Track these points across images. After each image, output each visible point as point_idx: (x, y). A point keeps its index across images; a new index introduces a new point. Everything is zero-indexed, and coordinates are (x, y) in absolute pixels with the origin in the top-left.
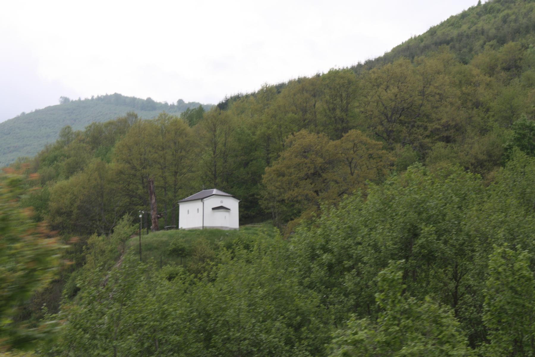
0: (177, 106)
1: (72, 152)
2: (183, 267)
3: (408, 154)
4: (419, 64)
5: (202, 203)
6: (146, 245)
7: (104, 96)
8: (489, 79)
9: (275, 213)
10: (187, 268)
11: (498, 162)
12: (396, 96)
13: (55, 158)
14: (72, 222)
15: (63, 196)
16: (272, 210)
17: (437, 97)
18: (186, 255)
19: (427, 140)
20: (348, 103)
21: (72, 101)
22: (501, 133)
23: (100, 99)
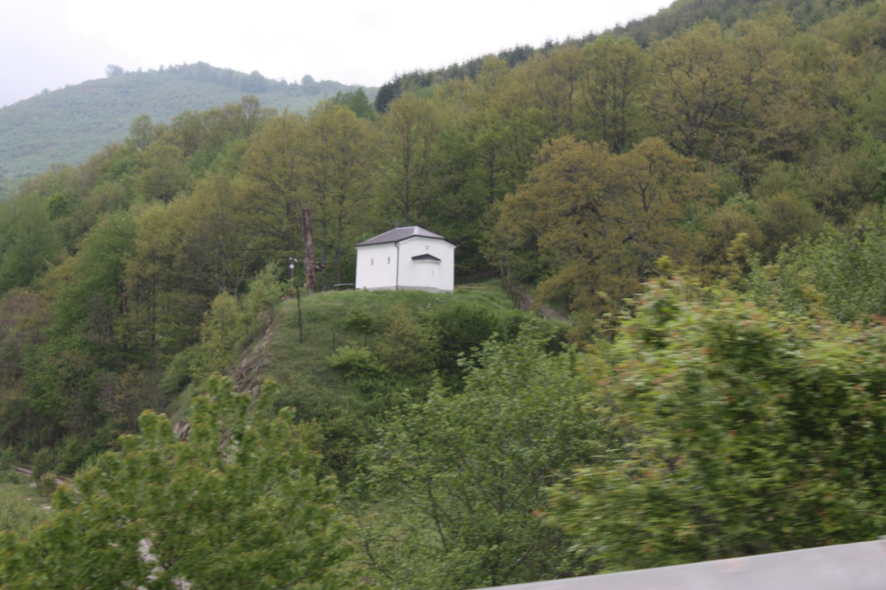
0: (301, 87)
1: (155, 159)
2: (369, 350)
3: (726, 180)
4: (744, 33)
5: (396, 249)
6: (308, 313)
7: (180, 67)
8: (853, 60)
9: (505, 268)
10: (376, 352)
11: (871, 196)
12: (704, 84)
13: (123, 168)
14: (175, 273)
15: (158, 230)
16: (500, 263)
17: (770, 87)
18: (373, 331)
19: (755, 157)
20: (626, 94)
21: (128, 74)
22: (875, 149)
23: (174, 71)
